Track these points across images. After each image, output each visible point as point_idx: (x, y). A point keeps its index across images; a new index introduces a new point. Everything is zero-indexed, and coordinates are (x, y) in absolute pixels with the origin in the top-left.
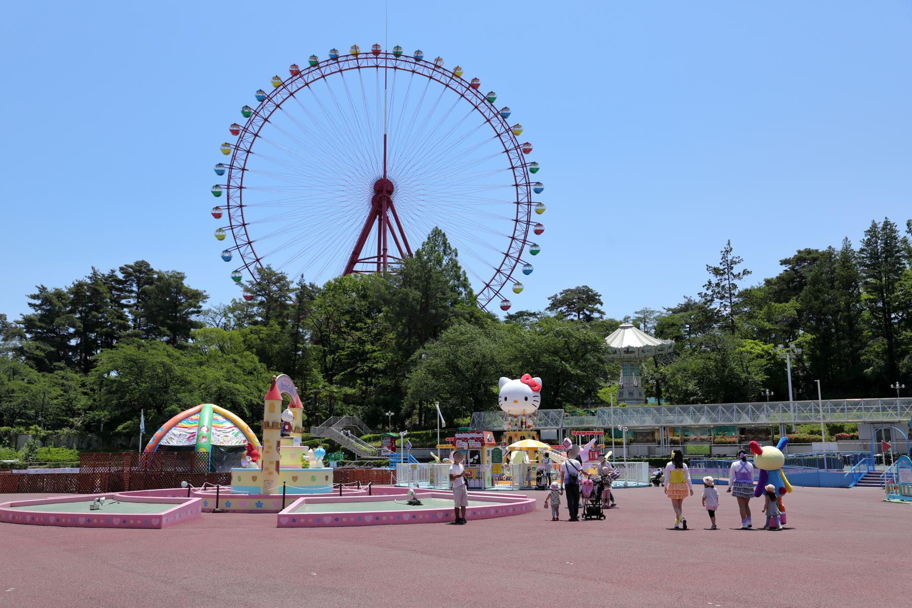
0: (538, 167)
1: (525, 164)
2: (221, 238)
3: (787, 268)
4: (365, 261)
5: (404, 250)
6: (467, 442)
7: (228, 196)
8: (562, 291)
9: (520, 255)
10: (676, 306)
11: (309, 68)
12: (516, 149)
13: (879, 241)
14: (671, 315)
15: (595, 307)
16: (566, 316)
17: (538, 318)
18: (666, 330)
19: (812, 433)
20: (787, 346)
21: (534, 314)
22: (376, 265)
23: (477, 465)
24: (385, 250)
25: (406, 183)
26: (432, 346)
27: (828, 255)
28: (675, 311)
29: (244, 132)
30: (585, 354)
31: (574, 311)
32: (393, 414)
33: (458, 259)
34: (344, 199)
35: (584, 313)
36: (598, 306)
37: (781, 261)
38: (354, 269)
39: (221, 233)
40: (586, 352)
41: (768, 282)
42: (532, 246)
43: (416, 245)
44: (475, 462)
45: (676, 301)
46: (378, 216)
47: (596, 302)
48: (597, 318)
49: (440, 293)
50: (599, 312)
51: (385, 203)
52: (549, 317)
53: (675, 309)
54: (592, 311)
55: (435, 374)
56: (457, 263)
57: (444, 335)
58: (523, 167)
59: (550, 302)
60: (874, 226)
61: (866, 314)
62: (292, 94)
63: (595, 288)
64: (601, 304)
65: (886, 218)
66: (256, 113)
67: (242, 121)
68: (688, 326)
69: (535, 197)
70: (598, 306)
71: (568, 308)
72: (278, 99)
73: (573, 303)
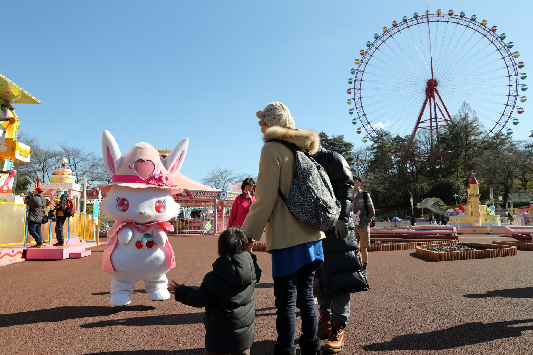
1: (517, 74)
2: (350, 104)
7: (354, 93)
9: (511, 114)
22: (430, 123)
39: (349, 101)
42: (519, 109)
62: (384, 42)
66: (367, 53)
67: (360, 57)
69: (520, 71)
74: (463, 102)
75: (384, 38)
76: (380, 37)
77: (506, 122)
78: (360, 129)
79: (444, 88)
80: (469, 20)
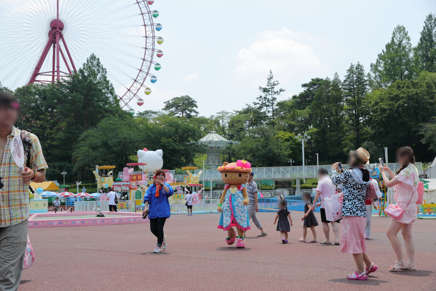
0: (161, 27)
1: (150, 11)
3: (305, 89)
4: (47, 74)
5: (72, 69)
6: (121, 187)
8: (173, 99)
9: (148, 71)
10: (241, 110)
12: (148, 13)
13: (354, 76)
14: (238, 115)
15: (193, 109)
16: (175, 114)
17: (158, 115)
18: (235, 125)
19: (314, 184)
20: (303, 134)
21: (155, 113)
22: (51, 77)
23: (127, 201)
24: (58, 67)
25: (74, 25)
26: (91, 131)
27: (327, 83)
28: (240, 113)
30: (188, 138)
31: (180, 111)
32: (66, 173)
33: (107, 75)
34: (28, 29)
35: (186, 113)
36: (195, 108)
37: (302, 85)
38: (36, 79)
40: (188, 136)
41: (294, 97)
43: (79, 66)
44: (125, 199)
45: (242, 107)
46: (53, 45)
47: (193, 105)
48: (194, 116)
49: (96, 98)
50: (195, 112)
51: (58, 36)
52: (164, 114)
53: (241, 111)
54: (191, 111)
55: (94, 148)
56: (106, 77)
57: (99, 125)
58: (151, 26)
59: (165, 105)
60: (352, 66)
61: (347, 117)
63: (193, 97)
64: (197, 107)
65: (358, 62)
68: (248, 122)
69: (157, 34)
70: (195, 108)
71: (176, 109)
73: (179, 106)
74: (91, 54)
77: (144, 80)
79: (72, 32)
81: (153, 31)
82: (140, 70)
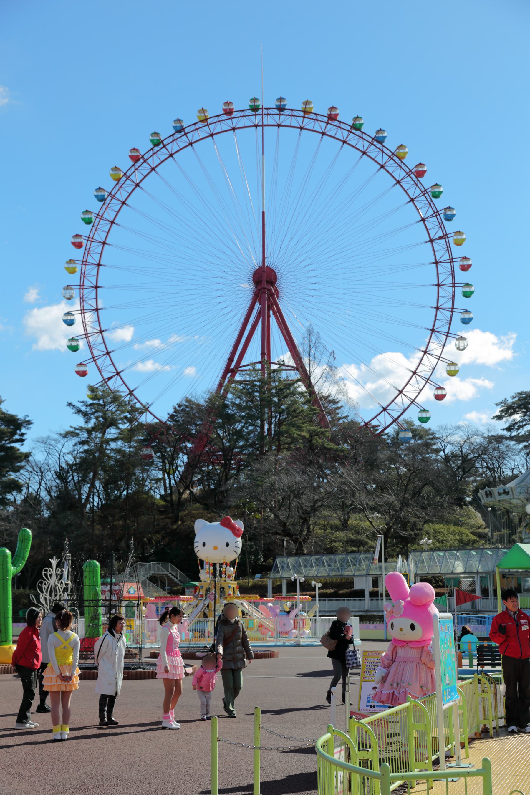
9: (453, 278)
11: (152, 149)
12: (409, 175)
25: (289, 263)
29: (89, 242)
67: (95, 206)
69: (461, 277)
72: (122, 195)
75: (173, 147)
76: (143, 157)
78: (85, 365)
80: (349, 128)
81: (441, 225)
82: (437, 308)
